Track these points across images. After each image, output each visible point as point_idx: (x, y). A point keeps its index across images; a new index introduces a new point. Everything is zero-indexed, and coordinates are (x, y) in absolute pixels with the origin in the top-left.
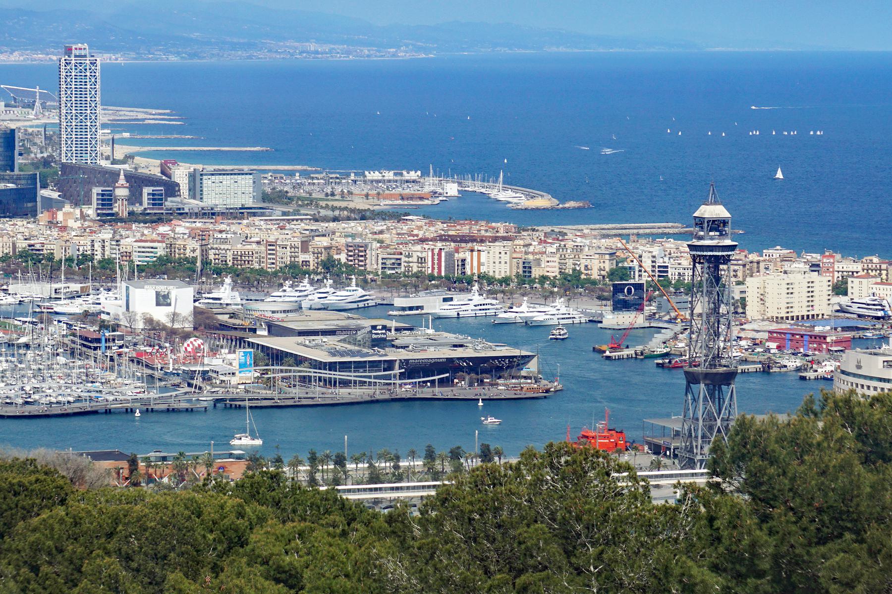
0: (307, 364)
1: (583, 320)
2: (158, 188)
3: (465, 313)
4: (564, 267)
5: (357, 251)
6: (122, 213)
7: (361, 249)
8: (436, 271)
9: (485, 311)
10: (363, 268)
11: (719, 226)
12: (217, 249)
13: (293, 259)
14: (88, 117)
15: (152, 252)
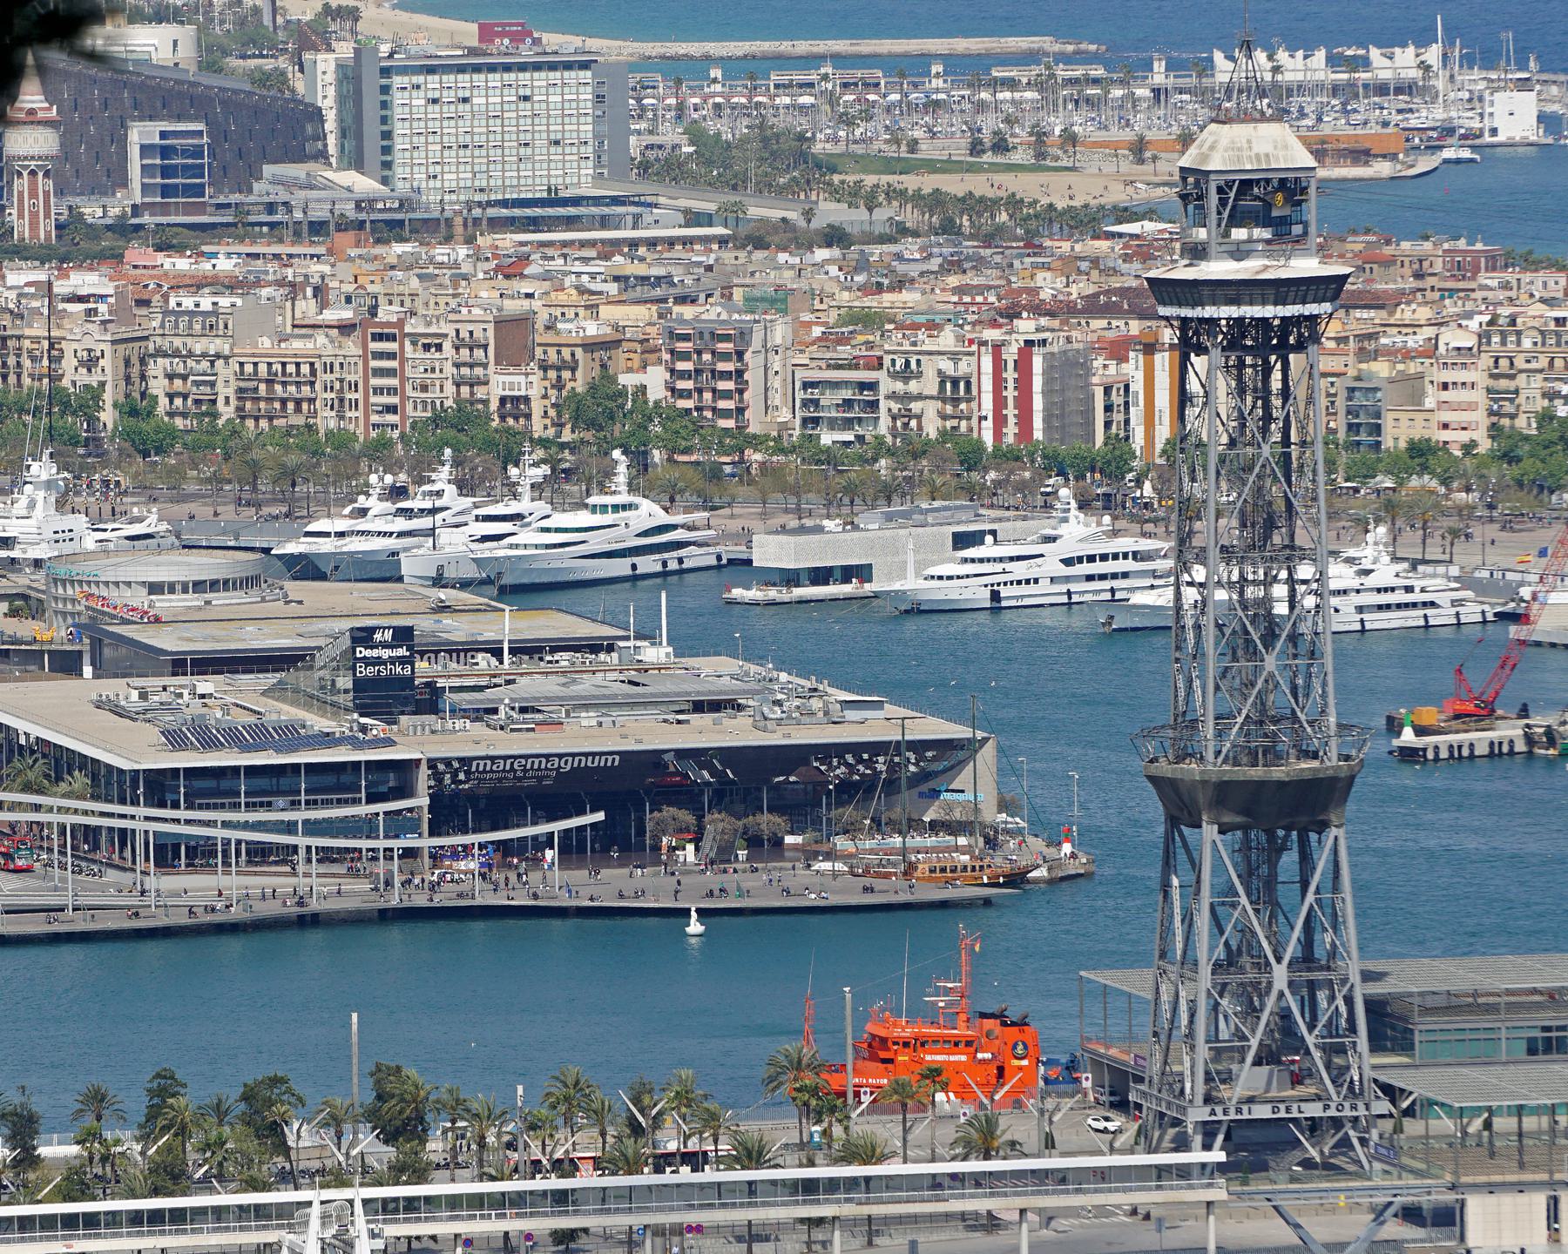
0: (80, 780)
1: (1471, 613)
2: (181, 127)
3: (1024, 590)
4: (1509, 408)
5: (707, 357)
6: (34, 225)
8: (1011, 430)
9: (1107, 584)
10: (730, 423)
11: (1269, 206)
12: (176, 354)
13: (465, 390)
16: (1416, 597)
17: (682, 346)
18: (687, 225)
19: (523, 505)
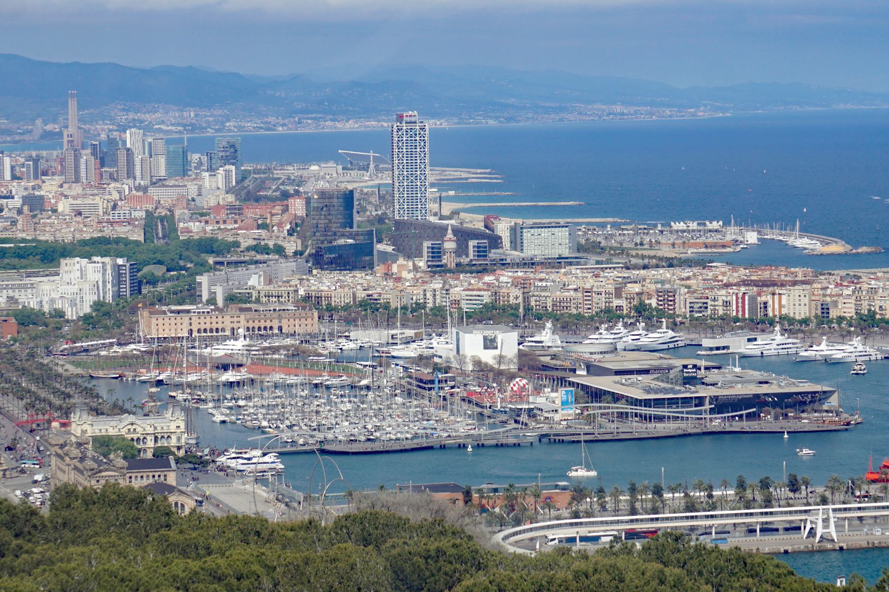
0: (624, 401)
1: (879, 357)
2: (482, 241)
3: (768, 352)
4: (860, 308)
5: (666, 296)
7: (670, 294)
8: (740, 313)
9: (786, 350)
10: (672, 312)
13: (607, 304)
14: (418, 178)
15: (478, 300)
16: (868, 353)
17: (660, 294)
18: (596, 264)
19: (640, 332)
